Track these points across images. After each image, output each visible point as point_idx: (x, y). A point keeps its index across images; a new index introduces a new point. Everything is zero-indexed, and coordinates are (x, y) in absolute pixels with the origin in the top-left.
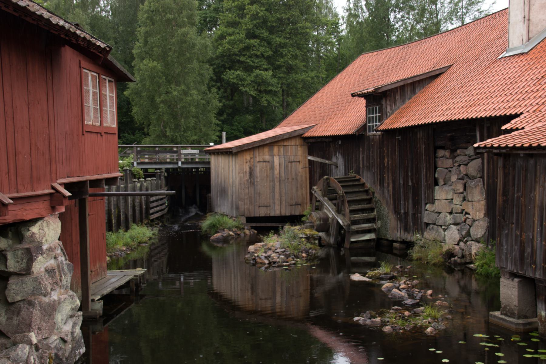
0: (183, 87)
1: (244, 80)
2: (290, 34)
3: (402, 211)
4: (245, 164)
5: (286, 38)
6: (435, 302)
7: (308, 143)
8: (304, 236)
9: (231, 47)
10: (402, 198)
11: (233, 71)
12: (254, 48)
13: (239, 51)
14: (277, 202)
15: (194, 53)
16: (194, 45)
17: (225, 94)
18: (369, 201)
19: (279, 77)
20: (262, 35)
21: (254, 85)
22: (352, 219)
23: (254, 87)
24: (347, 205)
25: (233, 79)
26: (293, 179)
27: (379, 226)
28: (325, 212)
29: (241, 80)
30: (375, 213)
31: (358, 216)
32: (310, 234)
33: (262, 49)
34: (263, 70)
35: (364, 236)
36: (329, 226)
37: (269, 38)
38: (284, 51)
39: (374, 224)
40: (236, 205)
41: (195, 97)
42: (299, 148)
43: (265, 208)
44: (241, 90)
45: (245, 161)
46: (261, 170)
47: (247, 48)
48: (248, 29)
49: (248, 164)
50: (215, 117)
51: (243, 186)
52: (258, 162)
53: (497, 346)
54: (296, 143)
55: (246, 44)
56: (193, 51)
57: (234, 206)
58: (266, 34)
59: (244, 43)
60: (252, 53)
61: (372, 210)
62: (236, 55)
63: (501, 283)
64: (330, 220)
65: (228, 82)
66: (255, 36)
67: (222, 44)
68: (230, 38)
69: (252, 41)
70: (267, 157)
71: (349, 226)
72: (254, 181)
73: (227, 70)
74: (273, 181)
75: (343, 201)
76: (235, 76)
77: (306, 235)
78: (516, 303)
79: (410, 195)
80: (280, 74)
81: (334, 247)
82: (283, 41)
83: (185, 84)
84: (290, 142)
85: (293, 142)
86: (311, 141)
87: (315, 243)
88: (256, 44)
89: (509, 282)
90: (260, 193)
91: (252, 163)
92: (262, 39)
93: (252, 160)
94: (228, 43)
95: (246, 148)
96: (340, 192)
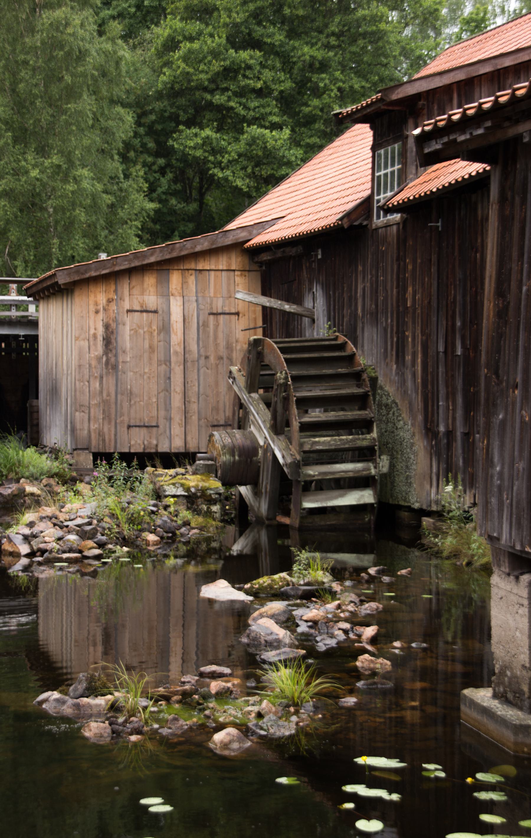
0: (56, 159)
1: (222, 151)
2: (338, 36)
3: (442, 429)
4: (92, 314)
5: (328, 47)
6: (356, 659)
7: (261, 264)
8: (180, 492)
9: (191, 70)
10: (442, 391)
11: (194, 130)
12: (248, 73)
13: (212, 80)
14: (177, 417)
15: (84, 75)
16: (82, 55)
17: (179, 187)
18: (362, 401)
19: (308, 145)
20: (269, 40)
21: (245, 163)
22: (307, 448)
23: (244, 168)
24: (294, 410)
25: (195, 148)
26: (221, 358)
27: (385, 470)
28: (251, 432)
29: (214, 152)
30: (375, 434)
31: (324, 441)
32: (196, 487)
33: (267, 74)
34: (266, 128)
35: (342, 496)
36: (259, 467)
37: (287, 47)
38: (323, 79)
39: (371, 465)
40: (71, 423)
41: (85, 184)
42: (238, 279)
43: (144, 431)
44: (213, 175)
45: (92, 308)
46: (135, 332)
47: (231, 72)
48: (236, 25)
49: (101, 315)
50: (138, 236)
51: (86, 372)
52: (128, 311)
53: (395, 797)
54: (230, 265)
55: (228, 63)
56: (80, 69)
57: (69, 427)
58: (277, 36)
59: (224, 60)
60: (242, 84)
61: (366, 425)
62: (205, 89)
63: (494, 591)
64: (260, 452)
65: (184, 158)
66: (253, 43)
67: (172, 63)
68: (188, 45)
69: (244, 55)
70: (151, 300)
71: (296, 466)
72: (117, 361)
73: (181, 127)
74: (167, 361)
75: (286, 400)
76: (200, 141)
77: (188, 490)
78: (524, 658)
79: (459, 384)
80: (311, 136)
81: (268, 527)
82: (319, 54)
83: (61, 152)
84: (213, 260)
85: (222, 262)
86: (265, 257)
87: (209, 514)
88: (252, 62)
89: (508, 588)
90: (131, 393)
91: (112, 315)
92: (270, 50)
93: (113, 307)
94: (185, 59)
95: (93, 274)
96: (280, 376)
